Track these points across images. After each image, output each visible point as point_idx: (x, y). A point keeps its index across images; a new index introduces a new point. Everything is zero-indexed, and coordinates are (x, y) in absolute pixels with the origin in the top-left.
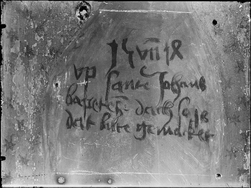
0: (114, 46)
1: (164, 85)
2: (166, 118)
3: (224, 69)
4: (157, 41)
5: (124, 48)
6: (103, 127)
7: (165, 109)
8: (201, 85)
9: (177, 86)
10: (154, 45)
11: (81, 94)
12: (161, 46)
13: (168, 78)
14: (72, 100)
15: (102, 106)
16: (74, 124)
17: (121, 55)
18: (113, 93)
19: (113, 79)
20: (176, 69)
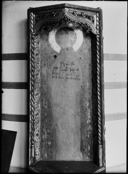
0: (61, 63)
1: (71, 70)
2: (71, 76)
3: (37, 135)
4: (69, 62)
5: (63, 63)
6: (59, 78)
7: (71, 74)
8: (78, 70)
9: (73, 70)
10: (68, 63)
11: (55, 72)
12: (70, 63)
13: (71, 69)
14: (53, 73)
15: (59, 52)
16: (54, 78)
17: (62, 64)
18: (61, 72)
19: (61, 69)
20: (73, 67)
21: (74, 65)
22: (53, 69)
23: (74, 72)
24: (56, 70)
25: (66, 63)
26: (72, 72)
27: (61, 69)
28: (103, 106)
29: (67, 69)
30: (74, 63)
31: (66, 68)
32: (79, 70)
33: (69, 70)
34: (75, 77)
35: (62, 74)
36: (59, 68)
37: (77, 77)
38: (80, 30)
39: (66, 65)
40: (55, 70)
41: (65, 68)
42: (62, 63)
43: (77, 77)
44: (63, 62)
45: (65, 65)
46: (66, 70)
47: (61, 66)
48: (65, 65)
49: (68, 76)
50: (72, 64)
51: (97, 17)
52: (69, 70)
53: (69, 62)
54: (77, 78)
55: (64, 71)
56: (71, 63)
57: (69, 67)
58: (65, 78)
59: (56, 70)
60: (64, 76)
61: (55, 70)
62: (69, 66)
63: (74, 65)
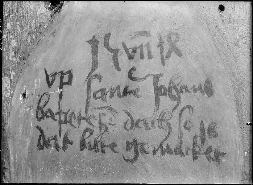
0: (94, 43)
1: (159, 91)
4: (146, 33)
5: (106, 44)
6: (83, 146)
8: (207, 89)
10: (144, 40)
11: (54, 106)
12: (154, 41)
14: (43, 113)
19: (96, 85)
21: (179, 54)
22: (39, 82)
23: (183, 104)
24: (61, 96)
25: (130, 45)
26: (166, 102)
27: (96, 85)
28: (251, 53)
29: (133, 85)
30: (179, 45)
31: (130, 76)
32: (219, 87)
33: (146, 87)
34: (188, 138)
35: (104, 120)
36: (79, 79)
37: (203, 141)
38: (103, 123)
39: (131, 58)
40: (55, 90)
41: (122, 79)
42: (101, 45)
43: (203, 141)
44: (107, 37)
45: (123, 58)
46: (126, 92)
47: (95, 65)
48: (123, 58)
49: (141, 135)
50: (167, 47)
51: (19, 130)
52: (146, 87)
53: (146, 33)
54: (204, 150)
55: (115, 102)
56: (161, 45)
57: (146, 67)
58: (121, 147)
59: (61, 96)
60: (117, 130)
61: (55, 90)
62: (146, 61)
63: (180, 55)
